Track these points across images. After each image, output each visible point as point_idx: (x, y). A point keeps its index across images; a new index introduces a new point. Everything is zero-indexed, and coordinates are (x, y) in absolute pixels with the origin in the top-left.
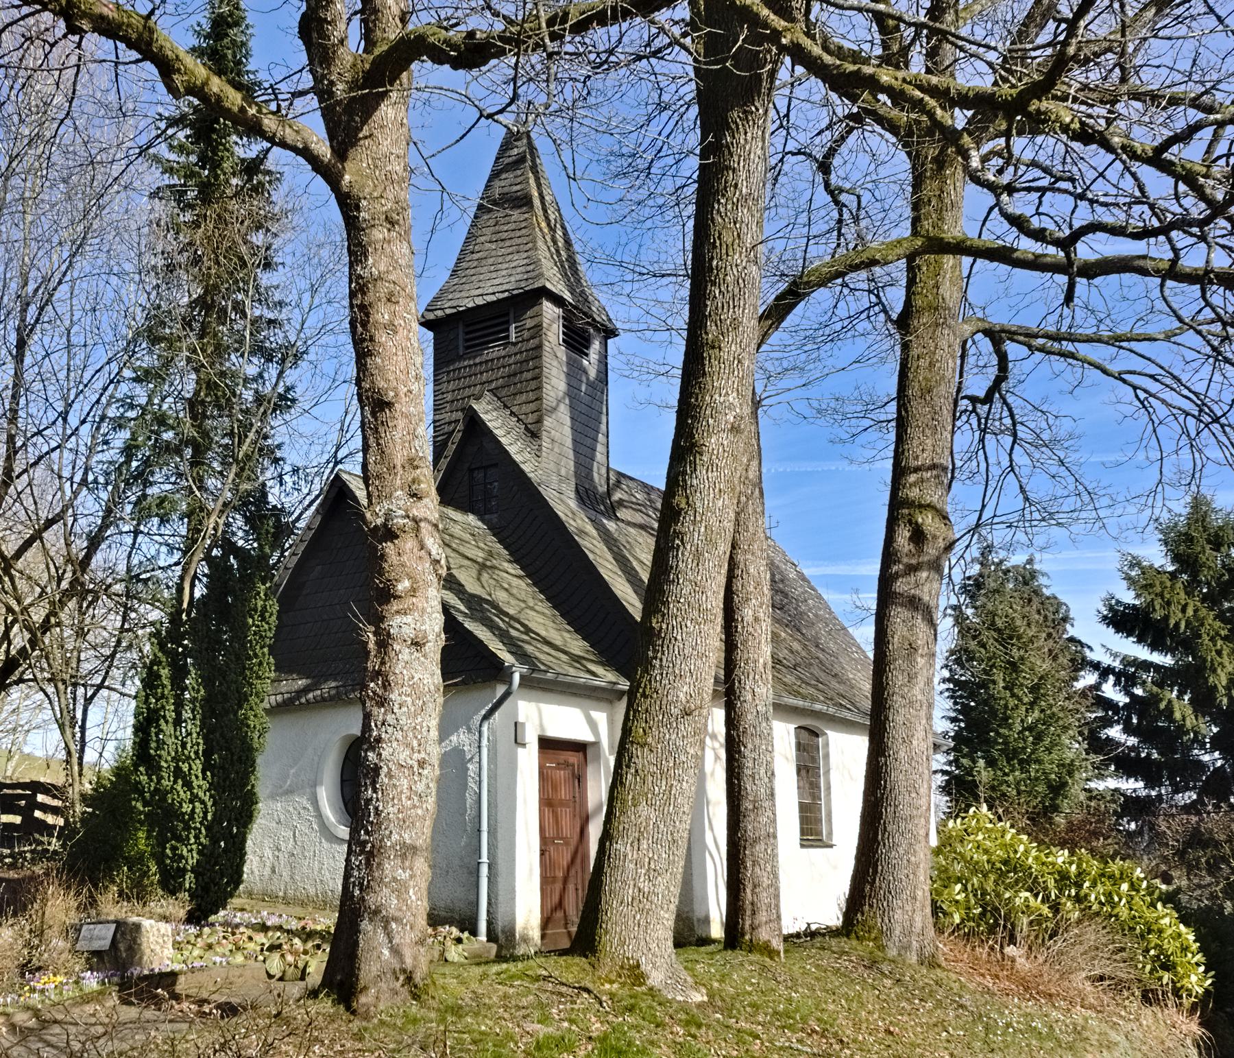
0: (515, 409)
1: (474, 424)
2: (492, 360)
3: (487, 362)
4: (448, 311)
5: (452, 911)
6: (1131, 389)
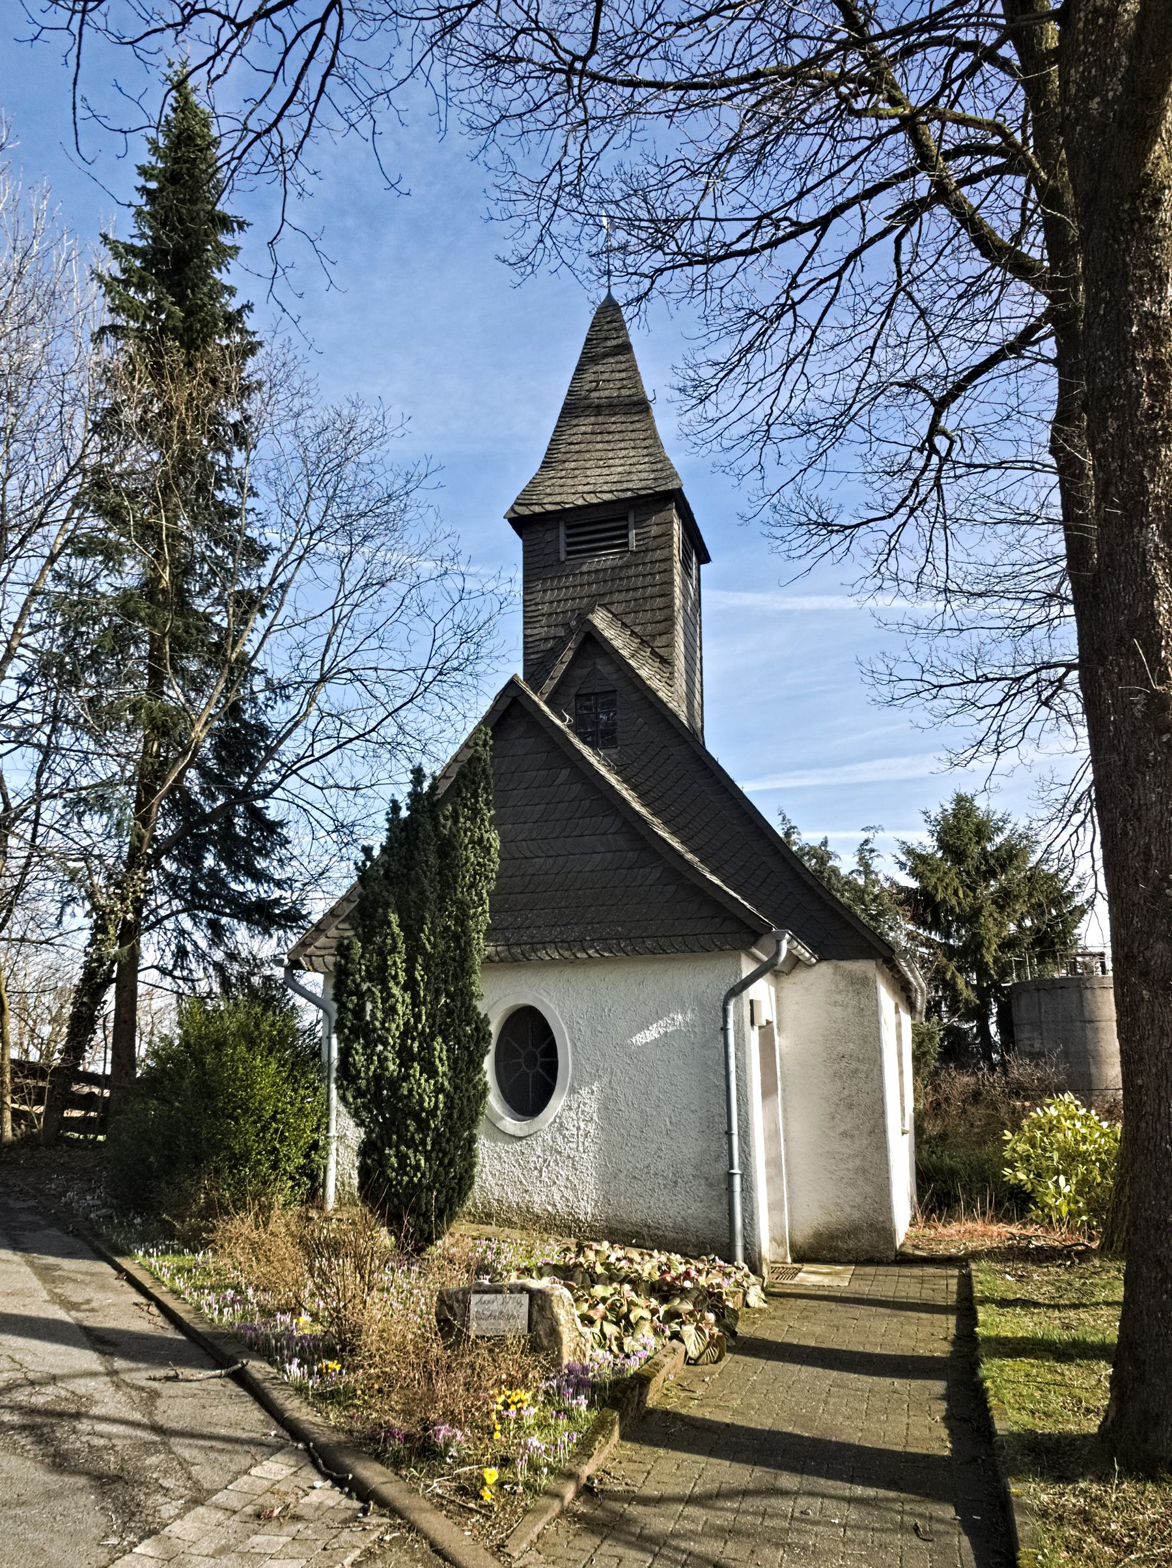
0: (637, 629)
1: (592, 641)
2: (605, 570)
3: (597, 571)
4: (549, 508)
5: (685, 1231)
6: (320, 15)
